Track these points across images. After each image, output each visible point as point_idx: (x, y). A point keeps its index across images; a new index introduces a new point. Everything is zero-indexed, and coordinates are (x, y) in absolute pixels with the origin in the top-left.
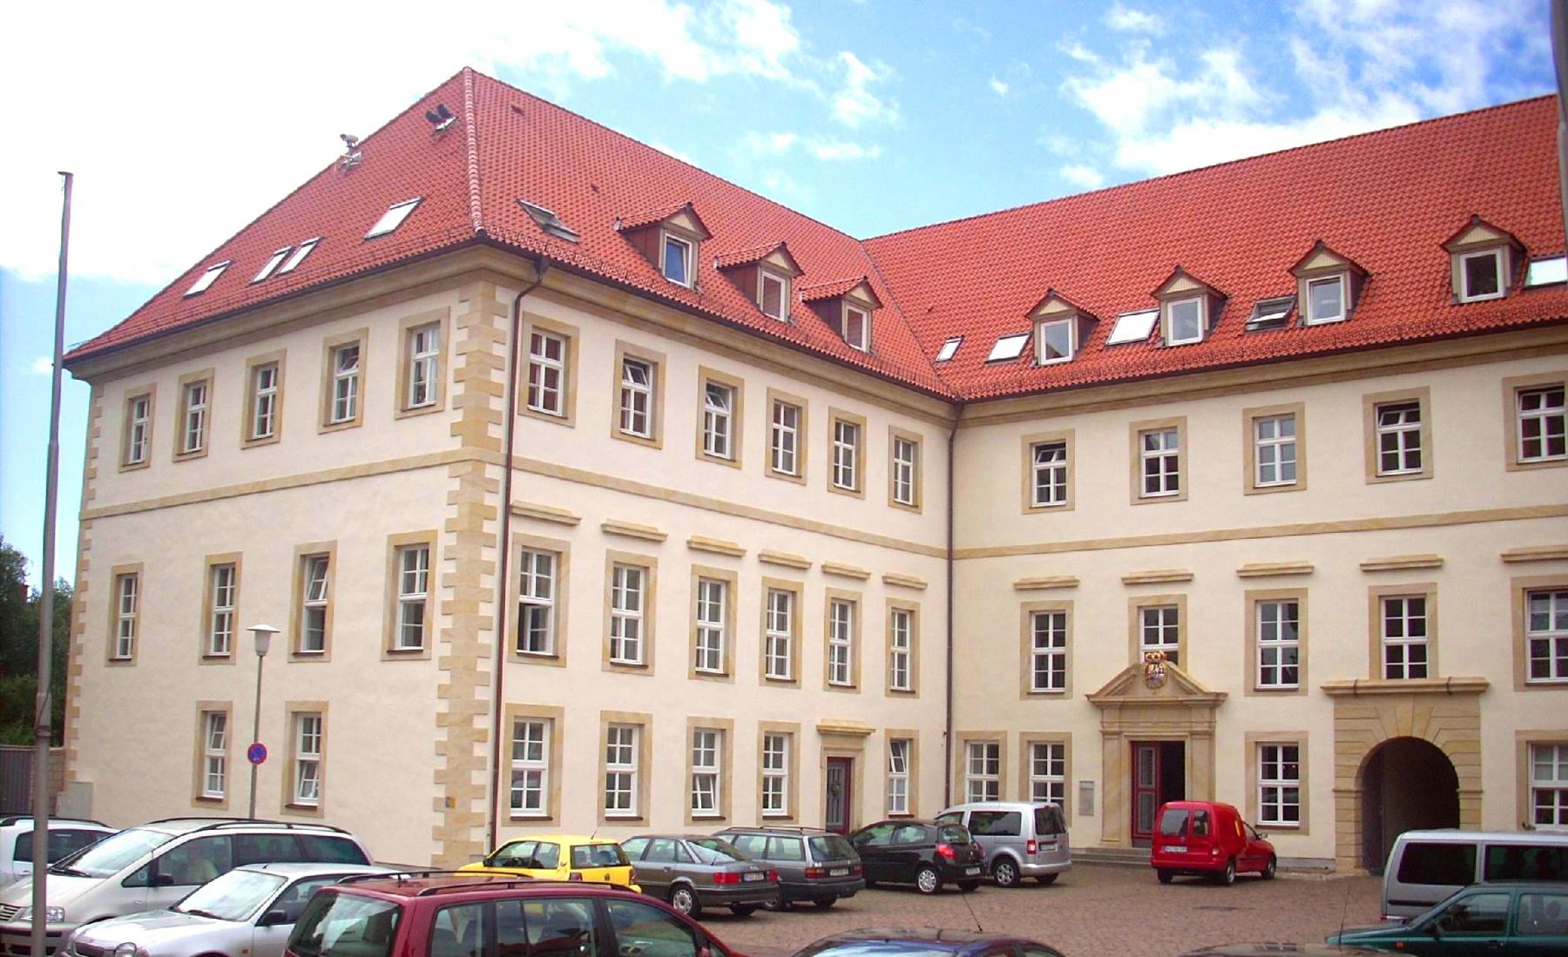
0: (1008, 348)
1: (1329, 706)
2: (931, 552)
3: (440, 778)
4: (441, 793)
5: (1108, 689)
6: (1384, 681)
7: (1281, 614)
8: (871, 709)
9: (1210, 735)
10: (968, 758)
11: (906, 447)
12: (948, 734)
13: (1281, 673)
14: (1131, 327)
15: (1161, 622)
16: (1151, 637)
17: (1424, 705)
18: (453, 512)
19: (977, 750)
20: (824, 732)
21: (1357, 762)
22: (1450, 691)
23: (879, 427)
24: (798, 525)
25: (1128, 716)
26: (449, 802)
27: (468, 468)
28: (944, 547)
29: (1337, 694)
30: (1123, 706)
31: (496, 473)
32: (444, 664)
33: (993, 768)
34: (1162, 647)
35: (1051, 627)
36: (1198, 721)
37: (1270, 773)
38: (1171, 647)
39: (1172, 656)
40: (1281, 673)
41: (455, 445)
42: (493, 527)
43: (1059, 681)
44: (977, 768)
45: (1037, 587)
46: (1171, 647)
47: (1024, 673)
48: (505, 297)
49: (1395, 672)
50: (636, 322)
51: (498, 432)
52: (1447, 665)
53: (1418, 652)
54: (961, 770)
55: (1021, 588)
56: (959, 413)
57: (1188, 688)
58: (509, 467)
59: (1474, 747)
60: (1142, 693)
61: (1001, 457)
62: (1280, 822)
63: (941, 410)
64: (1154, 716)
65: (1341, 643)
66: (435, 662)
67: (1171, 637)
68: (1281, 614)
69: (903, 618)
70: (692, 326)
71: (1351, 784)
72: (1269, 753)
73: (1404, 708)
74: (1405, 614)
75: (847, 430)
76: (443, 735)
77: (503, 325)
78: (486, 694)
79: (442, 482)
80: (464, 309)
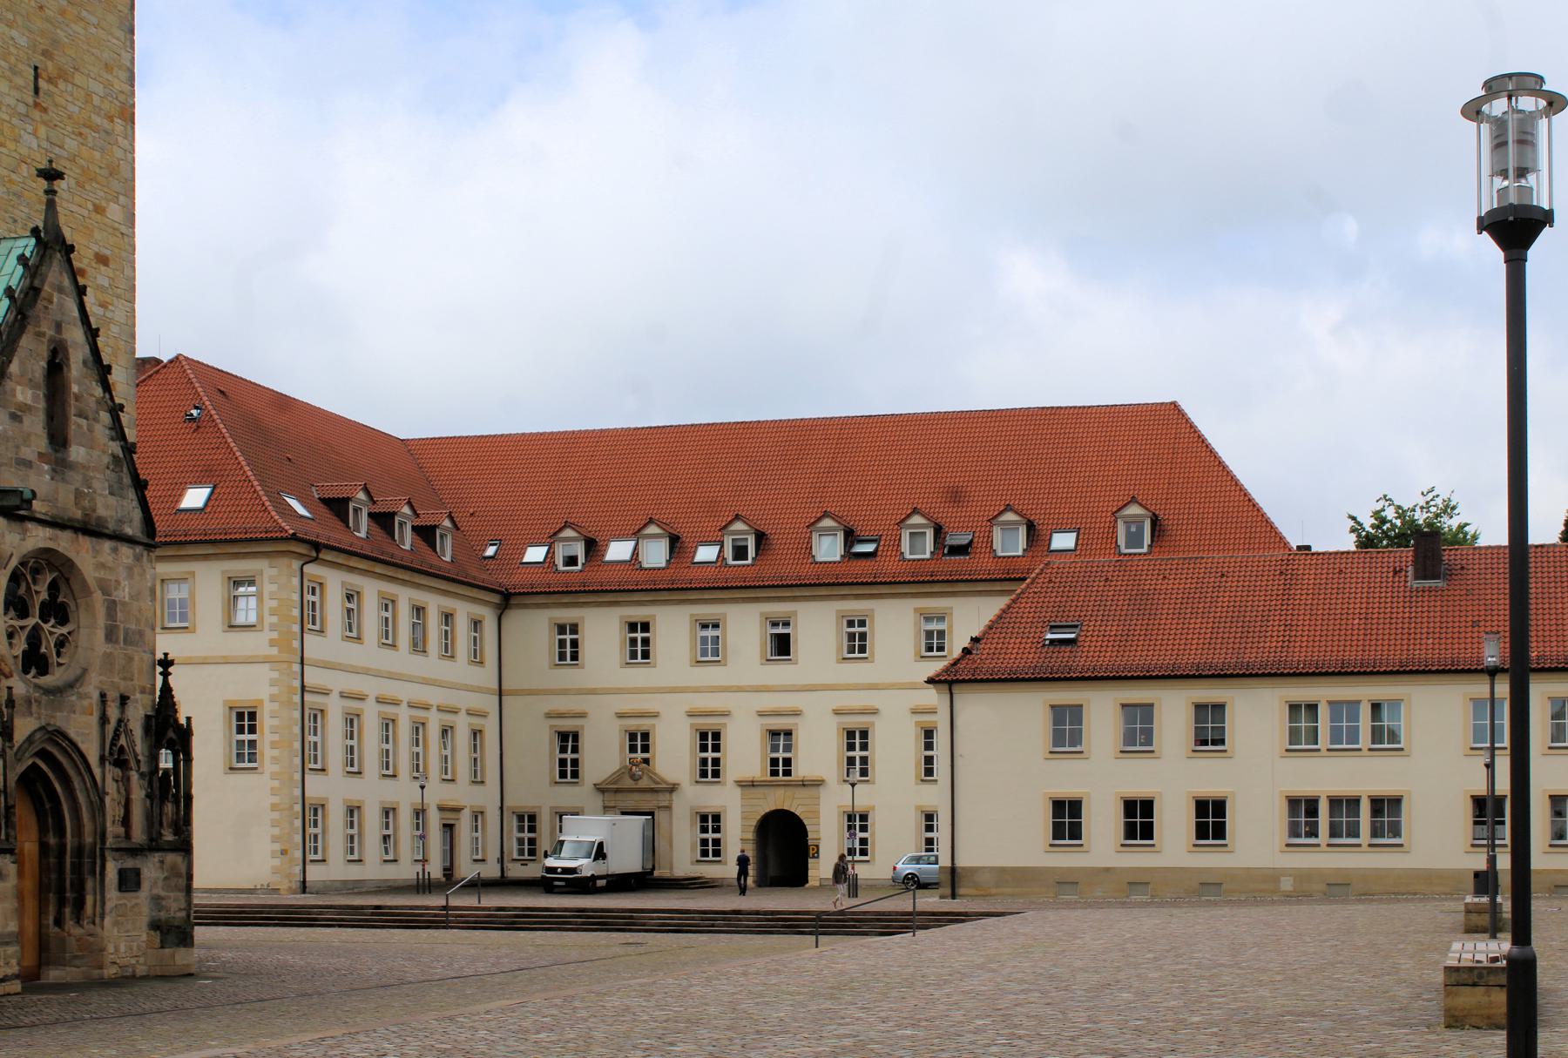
0: (535, 554)
1: (738, 791)
2: (487, 691)
3: (275, 839)
4: (277, 847)
5: (608, 781)
6: (769, 778)
7: (710, 740)
8: (462, 794)
9: (669, 808)
10: (515, 823)
11: (476, 624)
12: (502, 808)
13: (710, 770)
14: (619, 551)
15: (640, 741)
16: (633, 749)
17: (790, 791)
18: (275, 690)
19: (521, 818)
20: (441, 809)
21: (754, 823)
22: (804, 784)
23: (464, 611)
24: (426, 682)
25: (619, 796)
26: (284, 852)
27: (285, 666)
28: (496, 686)
29: (748, 785)
30: (617, 791)
31: (297, 668)
32: (273, 776)
33: (532, 829)
34: (640, 755)
35: (568, 740)
36: (663, 799)
37: (704, 830)
38: (645, 755)
39: (646, 761)
40: (710, 770)
41: (274, 651)
42: (297, 699)
43: (575, 774)
44: (521, 829)
45: (561, 716)
46: (645, 755)
47: (552, 770)
48: (296, 564)
49: (774, 773)
50: (351, 569)
51: (296, 644)
52: (801, 770)
53: (787, 762)
54: (510, 831)
55: (549, 716)
56: (506, 600)
57: (654, 777)
58: (302, 663)
59: (816, 814)
60: (628, 783)
61: (533, 630)
62: (711, 858)
63: (496, 599)
64: (636, 796)
65: (745, 754)
66: (267, 775)
67: (645, 749)
68: (710, 740)
69: (476, 734)
70: (379, 569)
71: (750, 836)
72: (704, 818)
73: (780, 792)
74: (780, 736)
75: (448, 617)
76: (276, 815)
77: (296, 581)
78: (298, 792)
79: (265, 672)
80: (274, 572)
